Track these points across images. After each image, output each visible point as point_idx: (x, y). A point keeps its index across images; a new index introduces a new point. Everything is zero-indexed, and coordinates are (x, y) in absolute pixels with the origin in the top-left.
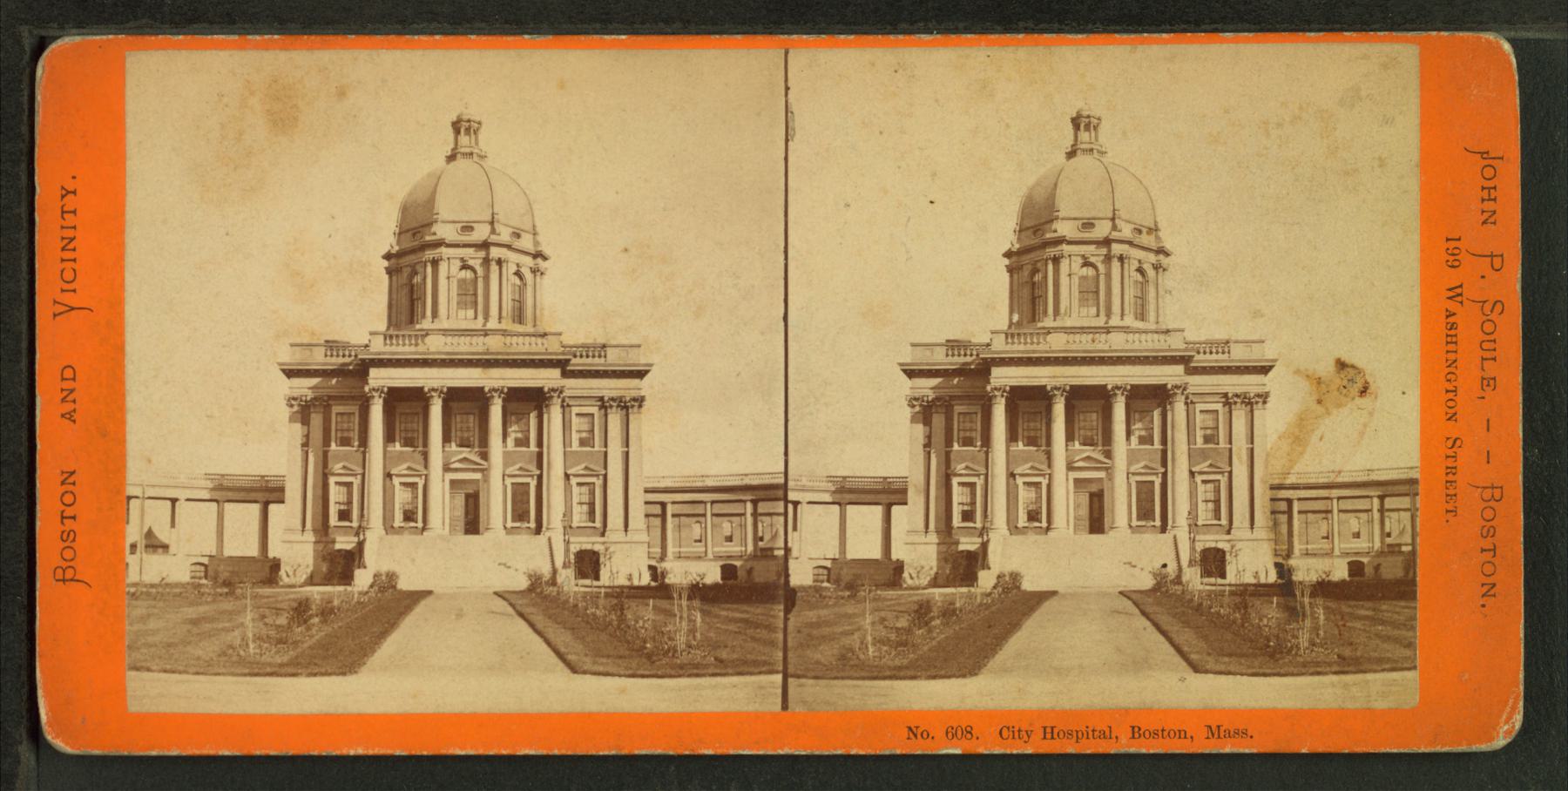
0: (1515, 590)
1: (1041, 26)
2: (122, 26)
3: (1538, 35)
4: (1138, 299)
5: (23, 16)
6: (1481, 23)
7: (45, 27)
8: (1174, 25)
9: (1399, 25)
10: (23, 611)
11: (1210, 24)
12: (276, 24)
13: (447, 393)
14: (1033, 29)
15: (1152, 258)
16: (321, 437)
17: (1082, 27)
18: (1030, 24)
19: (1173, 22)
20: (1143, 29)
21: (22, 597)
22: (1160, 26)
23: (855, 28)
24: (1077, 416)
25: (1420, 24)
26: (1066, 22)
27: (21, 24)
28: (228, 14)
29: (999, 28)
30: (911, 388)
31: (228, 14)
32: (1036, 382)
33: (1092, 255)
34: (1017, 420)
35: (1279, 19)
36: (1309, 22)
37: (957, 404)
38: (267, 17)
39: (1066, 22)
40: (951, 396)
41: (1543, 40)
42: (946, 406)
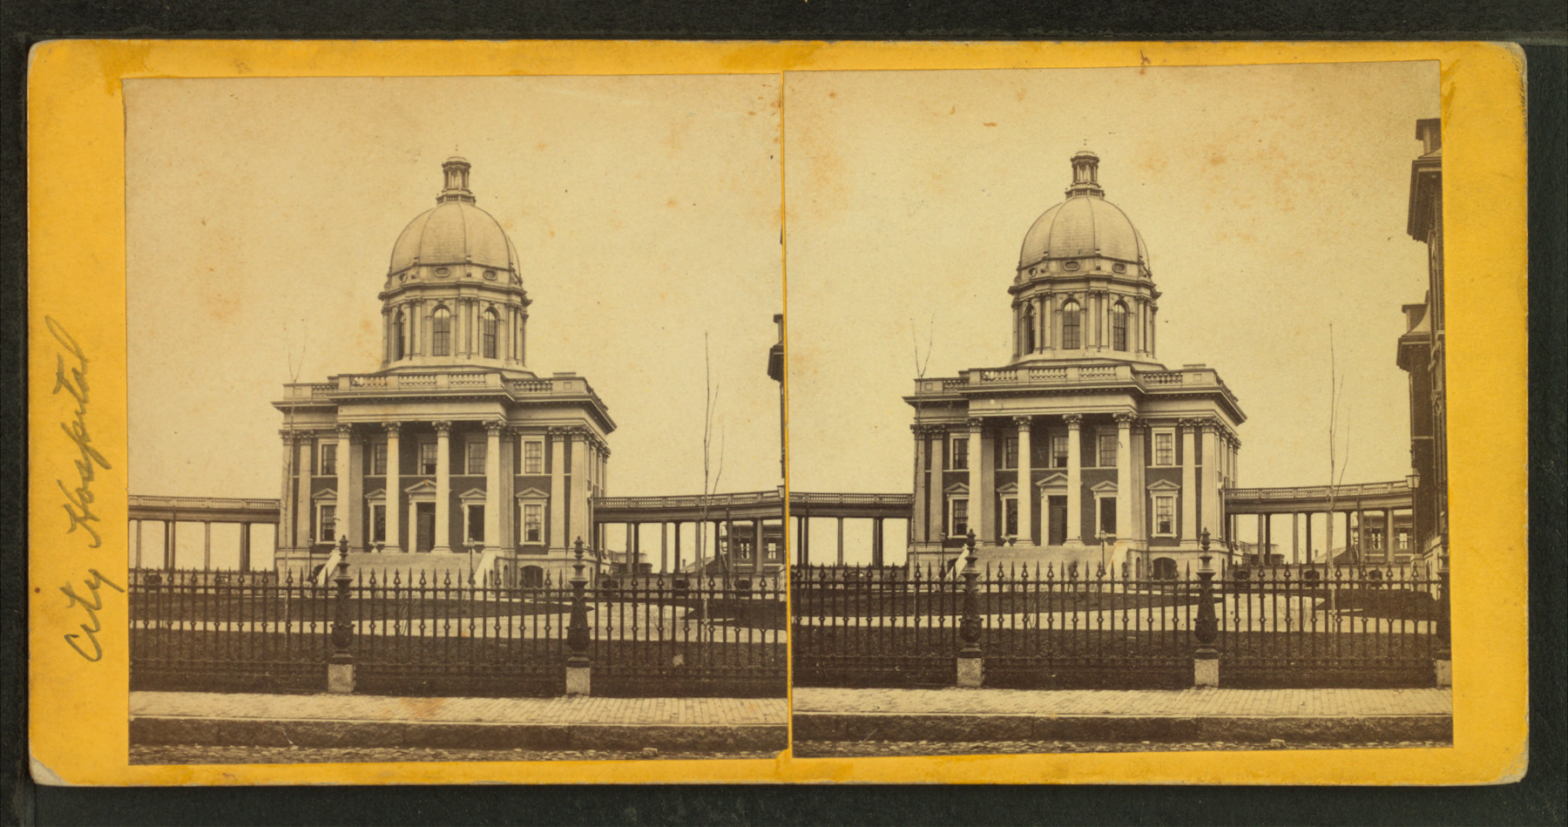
0: (363, 654)
1: (1052, 32)
2: (120, 32)
3: (1555, 42)
4: (1120, 330)
5: (20, 22)
6: (1496, 29)
7: (42, 33)
8: (1186, 32)
9: (1414, 32)
10: (19, 624)
11: (1223, 30)
12: (276, 31)
13: (452, 426)
14: (1043, 36)
15: (1132, 291)
16: (941, 460)
17: (1092, 34)
18: (1040, 31)
19: (1185, 29)
20: (1154, 36)
21: (19, 610)
22: (1171, 32)
23: (863, 33)
24: (420, 447)
25: (1436, 30)
26: (1076, 29)
27: (19, 30)
28: (228, 20)
29: (1008, 34)
30: (284, 424)
31: (228, 20)
32: (1004, 414)
33: (497, 302)
34: (370, 454)
35: (1292, 26)
36: (1322, 28)
37: (322, 438)
38: (268, 23)
39: (1076, 29)
40: (314, 430)
41: (1558, 47)
42: (312, 439)
